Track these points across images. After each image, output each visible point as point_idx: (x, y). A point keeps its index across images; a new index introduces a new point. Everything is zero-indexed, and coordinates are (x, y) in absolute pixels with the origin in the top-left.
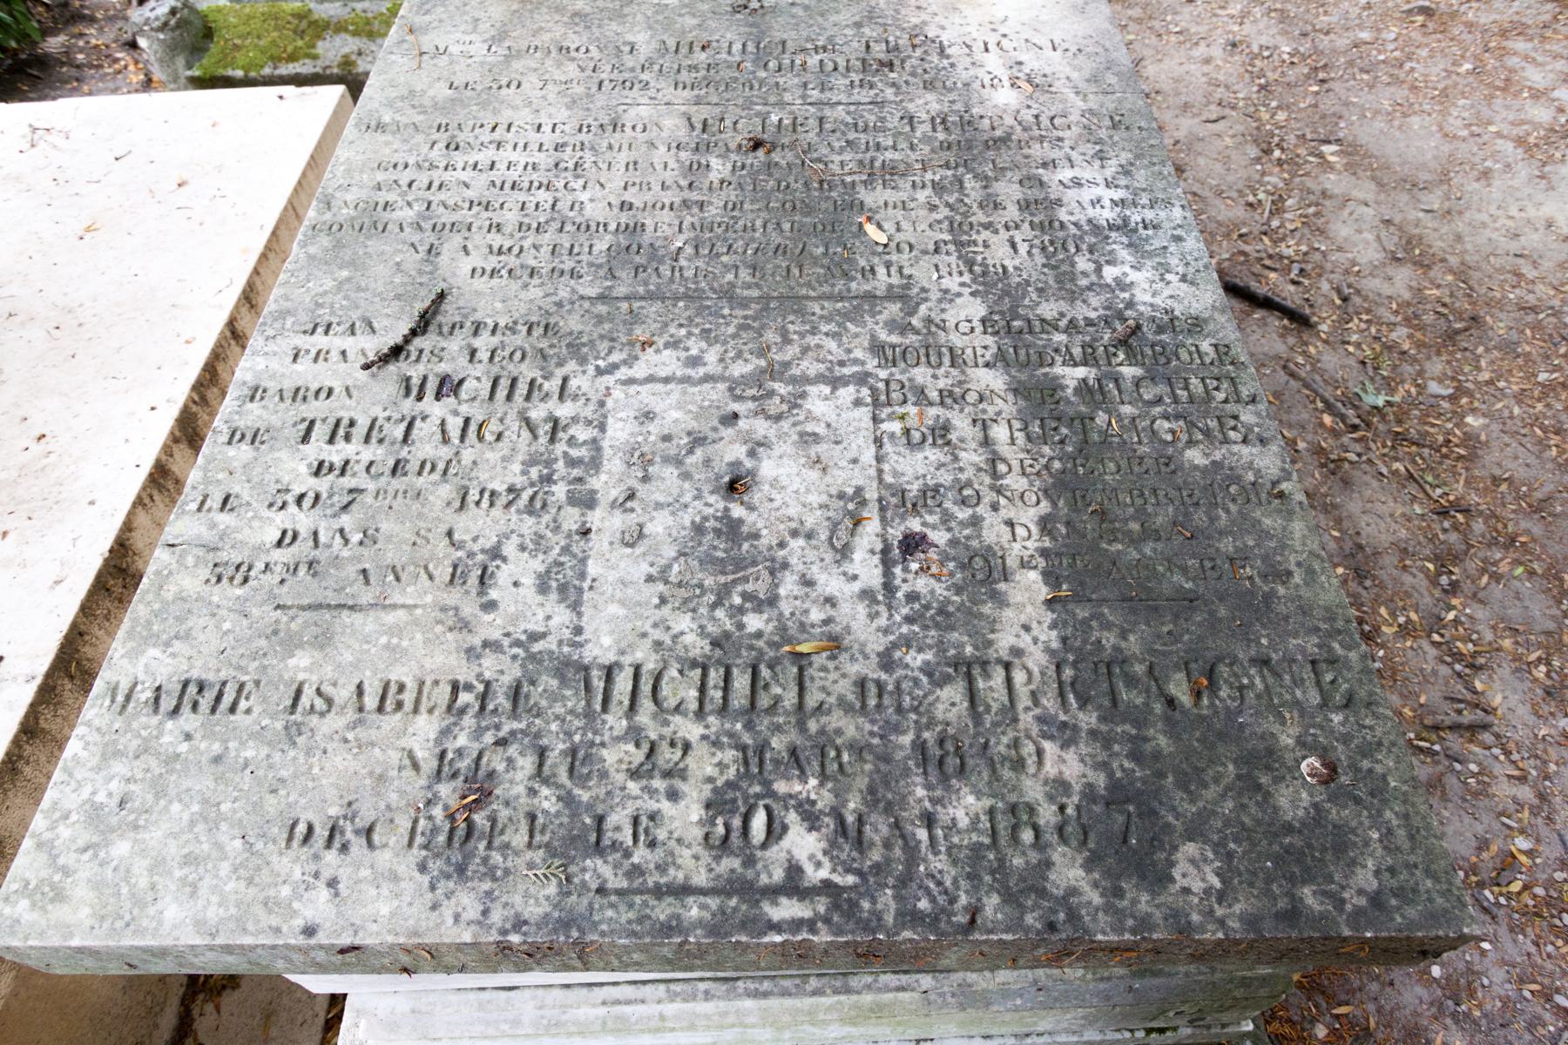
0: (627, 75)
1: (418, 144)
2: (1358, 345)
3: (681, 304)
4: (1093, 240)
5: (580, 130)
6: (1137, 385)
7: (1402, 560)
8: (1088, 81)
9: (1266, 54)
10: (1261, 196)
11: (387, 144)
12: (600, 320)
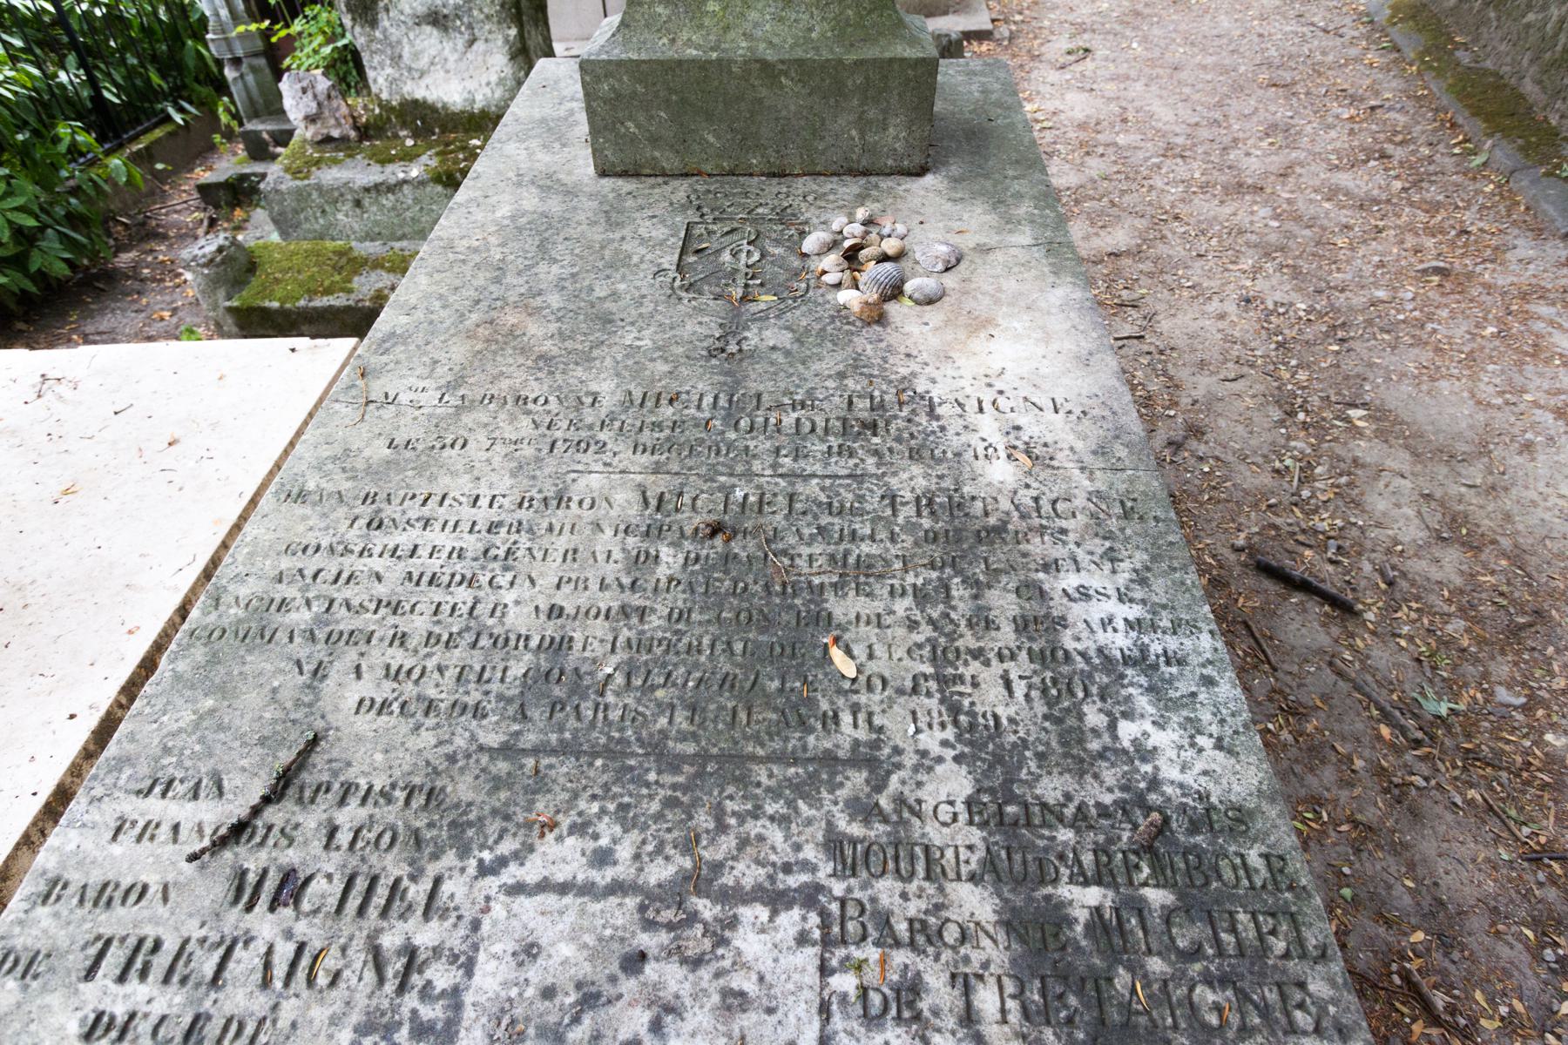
0: (584, 434)
1: (338, 521)
2: (1411, 639)
3: (599, 762)
4: (1105, 680)
5: (520, 505)
6: (1168, 922)
7: (1493, 924)
8: (1095, 453)
9: (1281, 310)
10: (1288, 462)
11: (305, 518)
12: (497, 783)
